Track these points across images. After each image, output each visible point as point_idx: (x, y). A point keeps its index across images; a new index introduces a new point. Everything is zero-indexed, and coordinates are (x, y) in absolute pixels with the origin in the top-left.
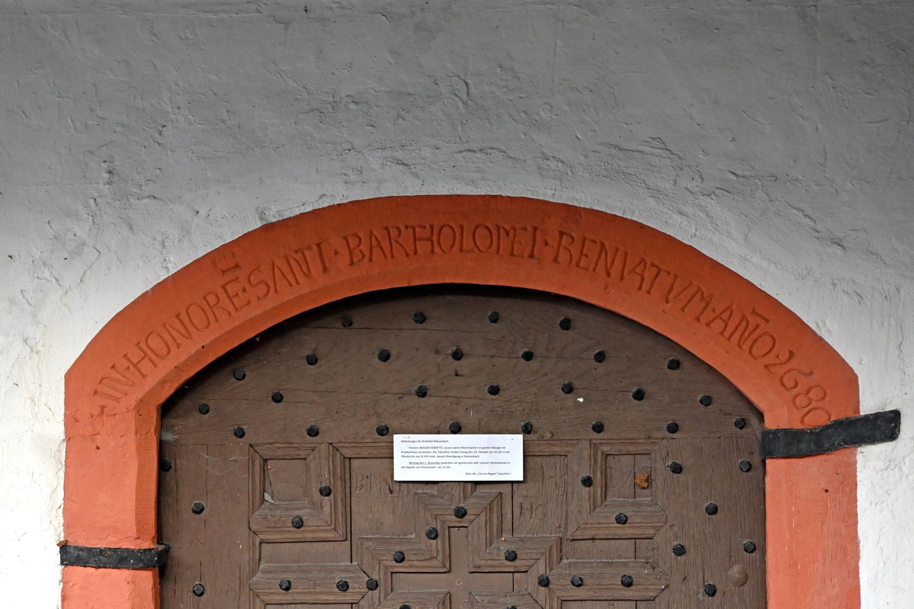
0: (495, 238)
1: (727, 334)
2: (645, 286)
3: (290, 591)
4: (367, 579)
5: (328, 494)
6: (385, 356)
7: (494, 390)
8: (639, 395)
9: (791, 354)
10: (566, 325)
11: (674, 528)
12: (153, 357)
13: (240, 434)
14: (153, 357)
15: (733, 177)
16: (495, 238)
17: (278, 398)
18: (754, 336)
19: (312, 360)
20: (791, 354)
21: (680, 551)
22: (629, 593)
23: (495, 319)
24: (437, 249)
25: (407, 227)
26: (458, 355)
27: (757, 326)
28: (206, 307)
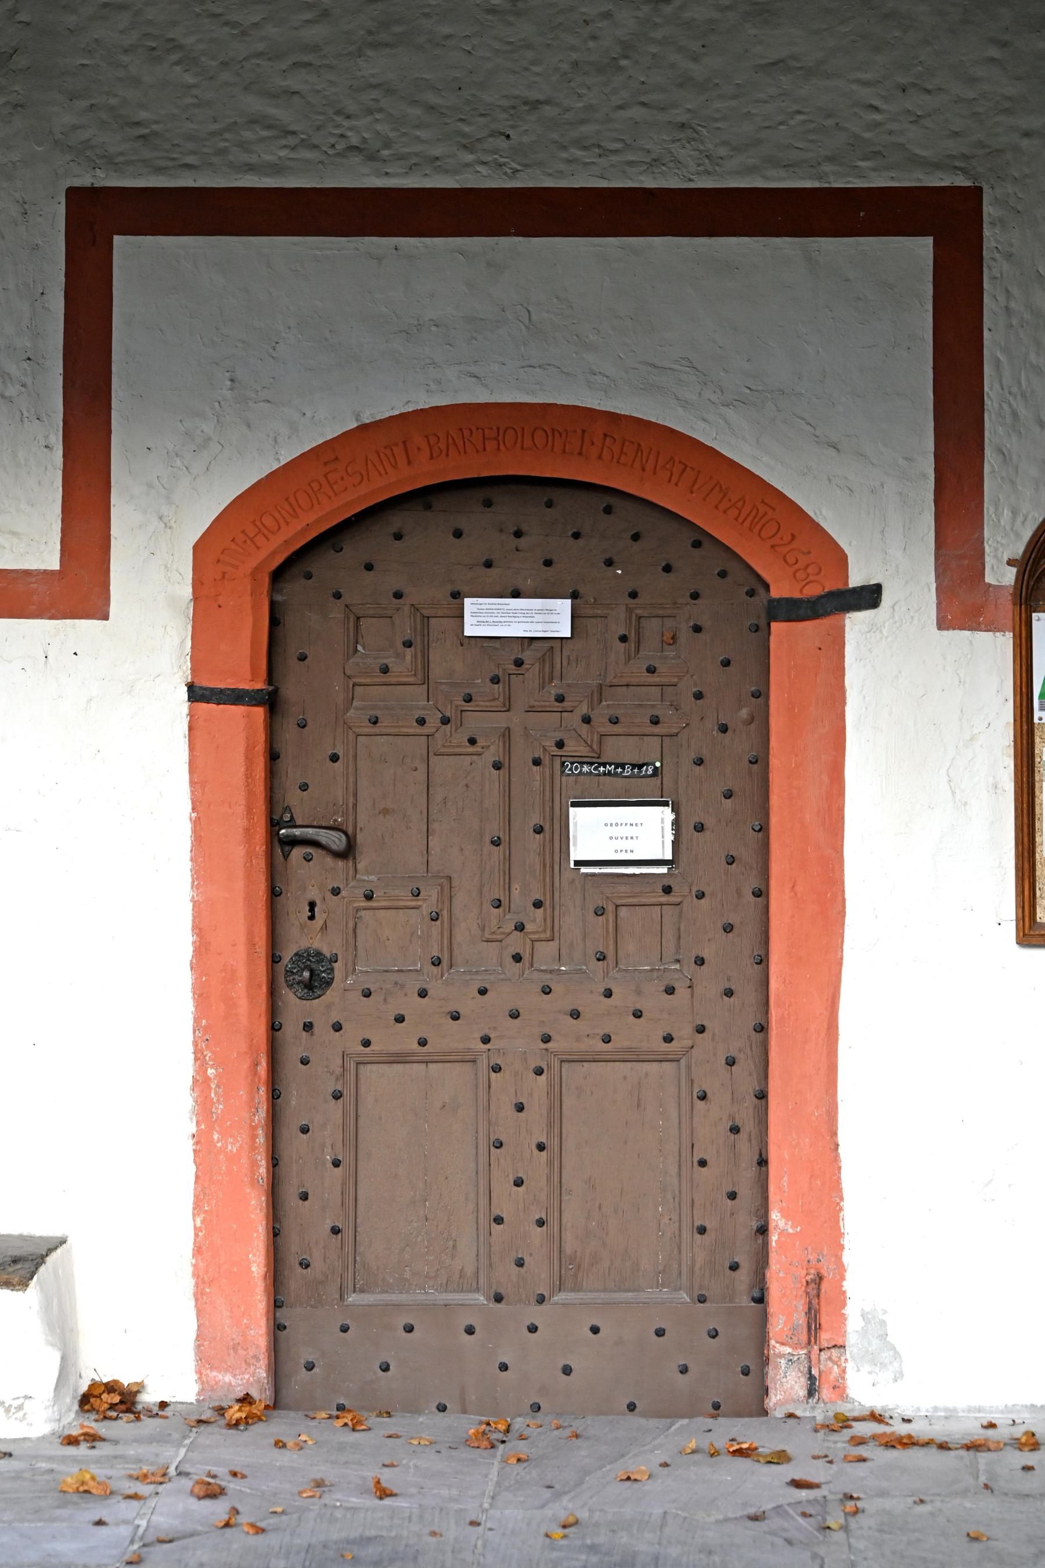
0: (519, 440)
1: (740, 520)
2: (674, 479)
3: (378, 725)
4: (441, 715)
5: (410, 646)
6: (458, 534)
7: (548, 563)
8: (667, 569)
9: (793, 537)
10: (608, 510)
11: (695, 677)
12: (266, 532)
13: (338, 596)
14: (266, 532)
15: (748, 391)
16: (550, 439)
17: (369, 567)
18: (763, 521)
19: (398, 537)
20: (793, 537)
21: (699, 696)
22: (656, 729)
23: (549, 504)
24: (502, 447)
25: (478, 429)
26: (518, 534)
27: (766, 514)
28: (311, 492)
